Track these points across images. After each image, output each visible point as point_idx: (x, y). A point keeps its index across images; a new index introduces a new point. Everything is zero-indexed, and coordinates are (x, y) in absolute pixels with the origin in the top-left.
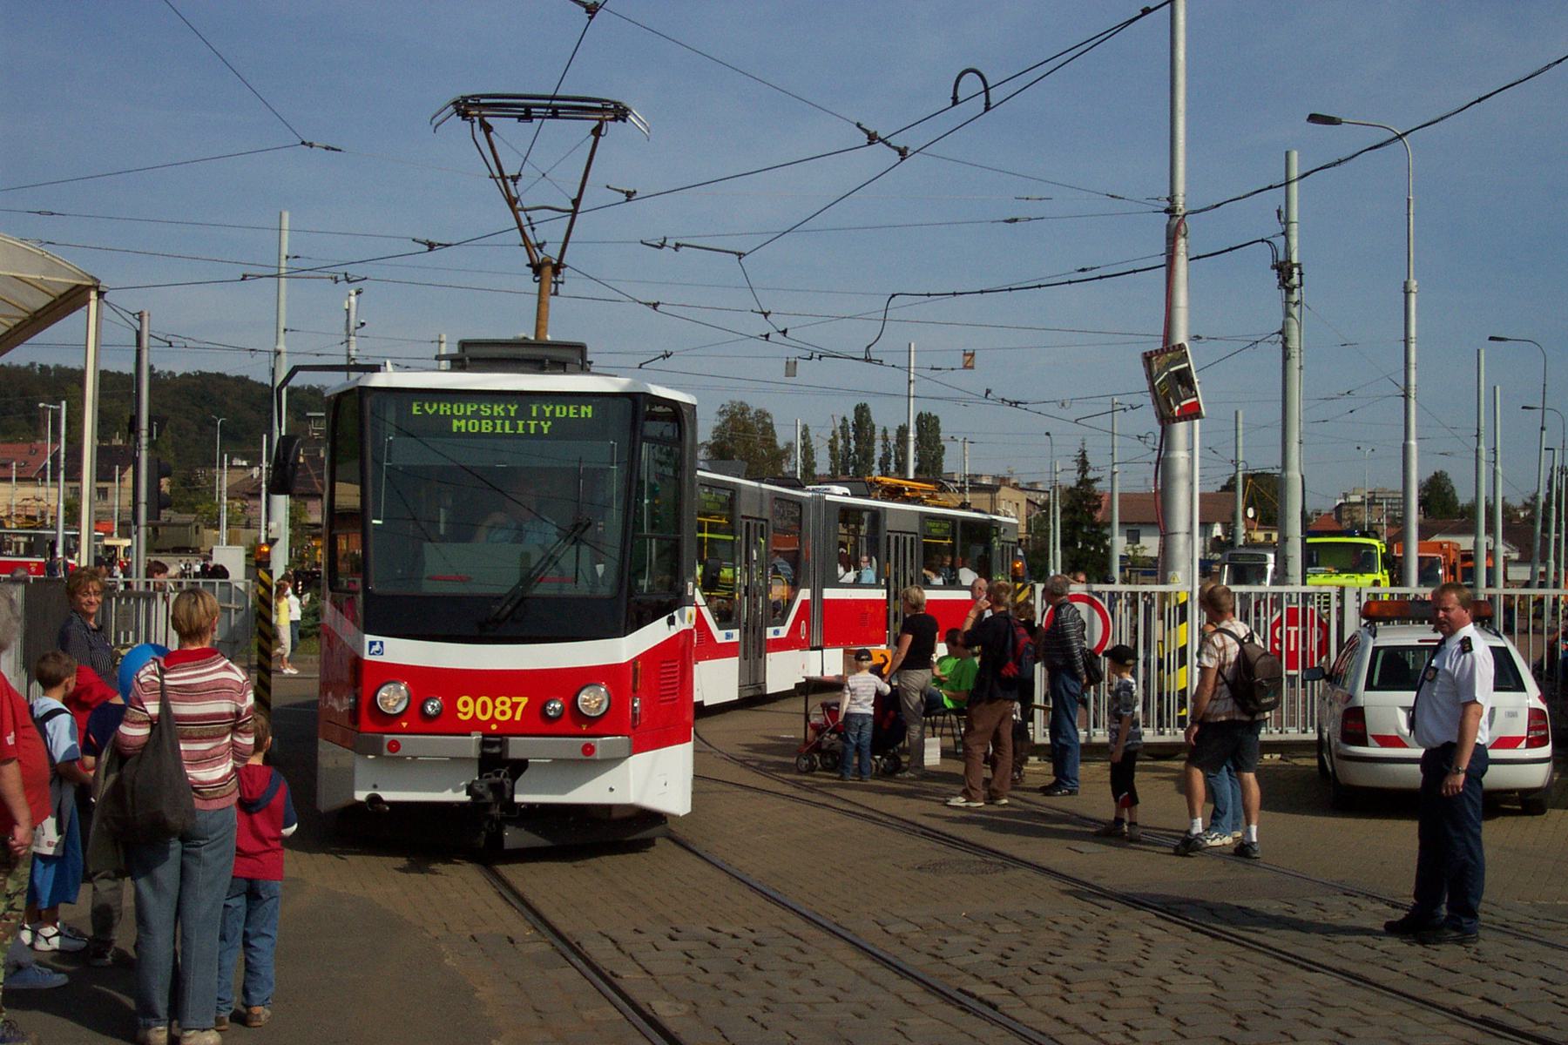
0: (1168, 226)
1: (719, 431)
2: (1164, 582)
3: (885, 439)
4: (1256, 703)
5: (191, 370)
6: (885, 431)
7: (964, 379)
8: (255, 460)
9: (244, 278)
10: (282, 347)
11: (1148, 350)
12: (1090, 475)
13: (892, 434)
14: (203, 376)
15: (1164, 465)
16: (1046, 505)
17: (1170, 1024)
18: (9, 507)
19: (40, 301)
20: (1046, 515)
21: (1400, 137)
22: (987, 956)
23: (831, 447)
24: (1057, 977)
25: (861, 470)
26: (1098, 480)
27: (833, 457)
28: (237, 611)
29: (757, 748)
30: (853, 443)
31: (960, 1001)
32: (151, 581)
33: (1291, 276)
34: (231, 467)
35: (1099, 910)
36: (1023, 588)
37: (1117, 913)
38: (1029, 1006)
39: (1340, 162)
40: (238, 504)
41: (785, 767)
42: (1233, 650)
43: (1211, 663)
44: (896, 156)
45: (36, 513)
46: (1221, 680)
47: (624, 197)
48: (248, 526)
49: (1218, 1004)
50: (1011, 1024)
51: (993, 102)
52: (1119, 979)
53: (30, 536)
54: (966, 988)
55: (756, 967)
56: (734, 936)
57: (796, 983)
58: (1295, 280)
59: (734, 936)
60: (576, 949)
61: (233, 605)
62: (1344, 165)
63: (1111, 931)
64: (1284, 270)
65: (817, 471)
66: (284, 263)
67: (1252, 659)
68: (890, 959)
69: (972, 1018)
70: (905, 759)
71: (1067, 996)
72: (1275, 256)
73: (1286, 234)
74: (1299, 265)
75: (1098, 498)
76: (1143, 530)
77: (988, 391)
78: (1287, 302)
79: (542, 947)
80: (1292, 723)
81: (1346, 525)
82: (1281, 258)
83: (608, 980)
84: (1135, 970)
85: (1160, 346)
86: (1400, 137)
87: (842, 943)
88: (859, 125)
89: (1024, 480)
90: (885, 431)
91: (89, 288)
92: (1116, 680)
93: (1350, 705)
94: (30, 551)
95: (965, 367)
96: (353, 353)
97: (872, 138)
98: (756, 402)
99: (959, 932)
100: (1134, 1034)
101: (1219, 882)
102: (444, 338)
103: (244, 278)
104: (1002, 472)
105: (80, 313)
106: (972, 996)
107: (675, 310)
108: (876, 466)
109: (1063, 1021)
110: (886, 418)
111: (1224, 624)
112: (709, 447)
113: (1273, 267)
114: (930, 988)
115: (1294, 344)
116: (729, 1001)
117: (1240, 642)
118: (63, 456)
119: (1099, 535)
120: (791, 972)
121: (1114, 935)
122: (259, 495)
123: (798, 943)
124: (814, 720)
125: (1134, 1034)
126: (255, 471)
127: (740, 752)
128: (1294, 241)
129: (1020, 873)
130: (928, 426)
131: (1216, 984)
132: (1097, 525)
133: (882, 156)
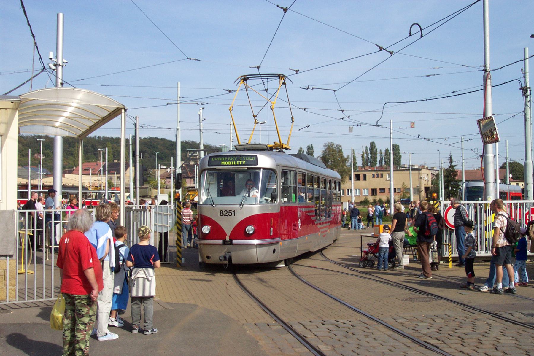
0: (484, 76)
1: (324, 152)
2: (486, 199)
3: (381, 153)
5: (146, 137)
6: (381, 151)
7: (411, 131)
8: (169, 166)
9: (168, 104)
10: (179, 127)
11: (479, 119)
12: (453, 164)
14: (150, 138)
15: (484, 157)
16: (438, 175)
18: (89, 183)
19: (105, 114)
20: (438, 179)
22: (433, 330)
24: (459, 337)
25: (373, 165)
26: (456, 165)
27: (363, 160)
28: (170, 215)
29: (345, 260)
30: (370, 155)
31: (425, 345)
32: (141, 206)
33: (527, 92)
34: (161, 168)
35: (471, 314)
36: (436, 203)
37: (477, 315)
38: (450, 347)
40: (163, 181)
41: (358, 266)
44: (389, 54)
45: (98, 185)
47: (295, 72)
48: (167, 188)
51: (424, 34)
52: (482, 338)
53: (96, 193)
55: (353, 334)
56: (344, 323)
57: (367, 339)
58: (528, 93)
59: (344, 323)
60: (291, 328)
63: (476, 321)
64: (524, 90)
65: (357, 165)
66: (179, 99)
69: (430, 351)
70: (397, 263)
71: (464, 344)
74: (529, 88)
75: (456, 172)
77: (419, 135)
78: (526, 101)
80: (481, 250)
82: (523, 86)
83: (303, 339)
84: (486, 335)
85: (482, 118)
88: (376, 45)
89: (430, 167)
90: (381, 151)
91: (122, 108)
95: (411, 127)
96: (202, 129)
97: (381, 49)
101: (513, 304)
103: (168, 104)
104: (423, 164)
105: (119, 116)
106: (430, 344)
108: (378, 163)
110: (381, 146)
112: (321, 158)
113: (520, 89)
114: (414, 341)
115: (528, 116)
116: (345, 345)
118: (107, 166)
119: (457, 185)
120: (365, 335)
121: (477, 323)
122: (170, 178)
123: (366, 326)
126: (169, 170)
127: (339, 261)
128: (528, 80)
129: (442, 301)
130: (396, 148)
131: (516, 340)
132: (456, 182)
133: (385, 54)
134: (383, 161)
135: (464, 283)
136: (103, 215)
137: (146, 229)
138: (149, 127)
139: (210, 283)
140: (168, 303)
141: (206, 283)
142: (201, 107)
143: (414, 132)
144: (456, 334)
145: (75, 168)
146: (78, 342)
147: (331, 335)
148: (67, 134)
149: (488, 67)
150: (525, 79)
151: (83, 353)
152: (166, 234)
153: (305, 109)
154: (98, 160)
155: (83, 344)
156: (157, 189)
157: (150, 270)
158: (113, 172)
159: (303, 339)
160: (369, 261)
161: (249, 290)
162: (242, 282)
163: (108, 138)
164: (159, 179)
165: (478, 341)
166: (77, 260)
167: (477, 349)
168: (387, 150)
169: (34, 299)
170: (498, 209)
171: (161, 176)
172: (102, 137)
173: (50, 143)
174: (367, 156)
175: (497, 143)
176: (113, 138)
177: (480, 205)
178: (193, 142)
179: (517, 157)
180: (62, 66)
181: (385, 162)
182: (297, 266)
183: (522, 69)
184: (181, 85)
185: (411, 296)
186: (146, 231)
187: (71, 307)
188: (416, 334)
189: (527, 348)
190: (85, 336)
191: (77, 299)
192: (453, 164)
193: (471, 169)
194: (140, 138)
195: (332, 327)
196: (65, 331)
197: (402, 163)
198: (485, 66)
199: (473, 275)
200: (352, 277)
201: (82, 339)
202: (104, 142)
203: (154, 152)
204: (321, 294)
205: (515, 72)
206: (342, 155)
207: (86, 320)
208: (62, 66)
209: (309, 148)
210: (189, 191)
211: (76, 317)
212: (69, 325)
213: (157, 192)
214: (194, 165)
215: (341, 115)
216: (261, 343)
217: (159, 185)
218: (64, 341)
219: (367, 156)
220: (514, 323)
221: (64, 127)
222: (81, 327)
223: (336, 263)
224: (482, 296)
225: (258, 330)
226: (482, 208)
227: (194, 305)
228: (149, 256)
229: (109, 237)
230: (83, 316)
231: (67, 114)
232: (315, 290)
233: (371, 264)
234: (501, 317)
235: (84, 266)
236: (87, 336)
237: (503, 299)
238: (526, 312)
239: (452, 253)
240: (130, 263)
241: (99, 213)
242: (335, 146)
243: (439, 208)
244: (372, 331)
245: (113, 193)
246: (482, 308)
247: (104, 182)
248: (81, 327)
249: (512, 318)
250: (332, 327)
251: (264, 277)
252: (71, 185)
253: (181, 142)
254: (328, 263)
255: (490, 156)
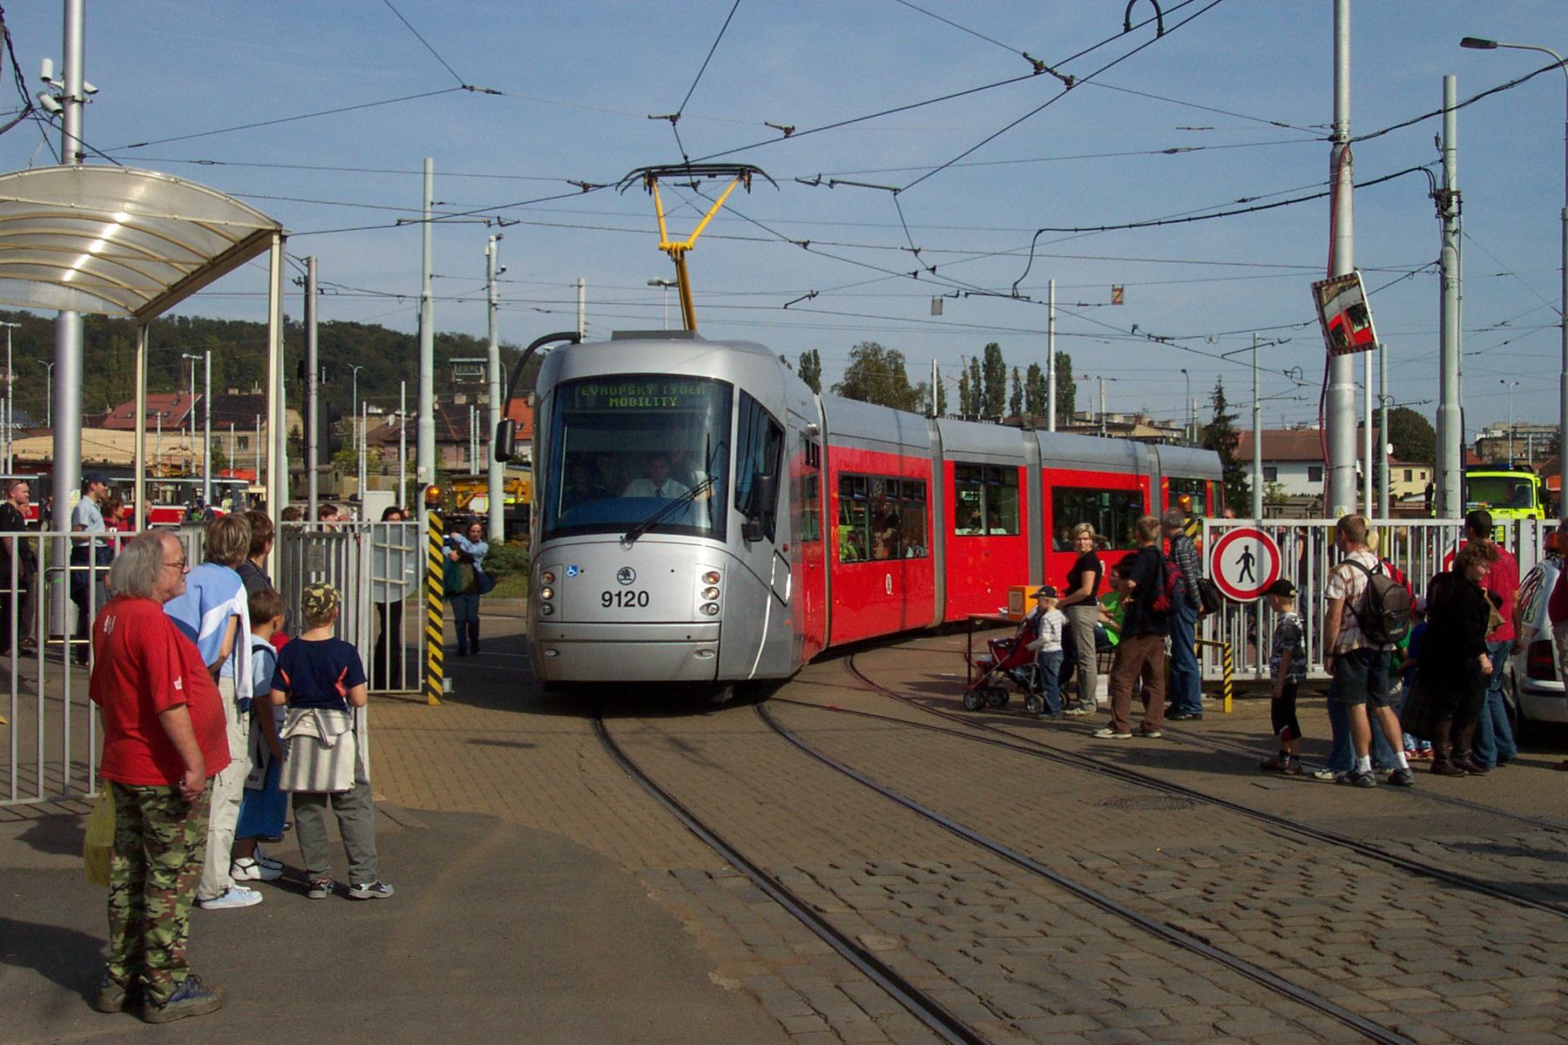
0: (1333, 154)
1: (852, 373)
3: (1016, 379)
4: (1385, 635)
6: (1016, 370)
9: (399, 223)
10: (428, 293)
12: (1228, 412)
13: (1023, 374)
15: (1329, 398)
17: (1389, 959)
18: (155, 456)
19: (220, 247)
21: (1561, 64)
23: (961, 388)
26: (1235, 417)
27: (963, 397)
28: (408, 552)
29: (921, 686)
36: (1189, 525)
37: (1313, 849)
39: (1513, 84)
40: (375, 452)
41: (962, 706)
42: (1362, 582)
43: (1338, 595)
45: (181, 462)
46: (1348, 611)
47: (782, 134)
48: (385, 473)
49: (1436, 939)
50: (1228, 959)
53: (177, 484)
54: (1174, 922)
55: (959, 902)
56: (931, 872)
57: (1000, 918)
58: (1454, 209)
59: (931, 872)
60: (776, 884)
61: (404, 547)
62: (1517, 87)
64: (1442, 198)
66: (429, 208)
67: (1381, 592)
68: (1093, 894)
69: (1183, 951)
71: (1280, 931)
72: (1433, 183)
73: (1444, 161)
74: (1457, 193)
76: (1279, 467)
77: (1135, 327)
78: (1446, 231)
79: (741, 882)
81: (1487, 460)
82: (1439, 186)
83: (813, 917)
84: (1342, 904)
85: (1324, 277)
86: (1561, 64)
87: (1041, 879)
88: (1025, 55)
90: (1016, 370)
91: (271, 232)
92: (1274, 616)
93: (1536, 639)
94: (177, 499)
95: (1114, 302)
96: (494, 299)
97: (1039, 68)
98: (888, 343)
99: (1157, 867)
100: (1354, 968)
101: (1412, 818)
102: (583, 282)
103: (399, 223)
104: (1136, 409)
105: (261, 259)
106: (1183, 930)
107: (824, 249)
108: (1007, 405)
109: (1278, 955)
110: (1016, 359)
111: (1353, 555)
115: (1453, 274)
117: (1369, 573)
122: (398, 442)
123: (996, 878)
124: (976, 658)
125: (1354, 968)
126: (391, 419)
128: (1453, 169)
130: (1063, 364)
131: (1429, 919)
132: (1234, 463)
134: (1023, 401)
135: (1269, 754)
136: (225, 547)
137: (327, 593)
138: (340, 290)
139: (533, 752)
140: (411, 811)
141: (500, 749)
142: (497, 229)
143: (1120, 318)
144: (1258, 904)
145: (109, 410)
146: (152, 924)
147: (895, 904)
148: (98, 306)
149: (1344, 128)
150: (1445, 167)
151: (169, 958)
152: (397, 607)
153: (805, 245)
154: (180, 387)
155: (169, 929)
156: (356, 474)
157: (336, 717)
158: (225, 424)
159: (813, 917)
160: (992, 691)
161: (646, 773)
162: (629, 751)
163: (211, 322)
164: (364, 446)
165: (1320, 922)
166: (134, 675)
167: (1317, 946)
168: (1034, 370)
169: (10, 797)
170: (1349, 545)
171: (369, 437)
172: (190, 318)
173: (39, 338)
174: (977, 386)
175: (1369, 352)
176: (223, 323)
177: (1316, 530)
178: (463, 337)
179: (1419, 398)
180: (82, 103)
181: (1028, 403)
182: (783, 705)
183: (1437, 139)
184: (435, 167)
185: (1122, 793)
186: (328, 600)
187: (132, 822)
188: (1143, 903)
189: (1461, 942)
190: (173, 908)
191: (145, 800)
192: (1228, 412)
193: (1279, 427)
194: (320, 325)
195: (898, 883)
196: (116, 890)
197: (1077, 409)
198: (1336, 126)
199: (1294, 732)
200: (944, 736)
201: (165, 916)
202: (201, 333)
203: (357, 365)
204: (859, 785)
205: (1417, 145)
206: (904, 380)
207: (176, 859)
208: (82, 103)
209: (806, 359)
210: (455, 482)
211: (147, 854)
212: (127, 875)
213: (357, 484)
214: (468, 404)
215: (912, 263)
216: (692, 927)
217: (363, 464)
218: (111, 923)
219: (977, 386)
220: (1419, 871)
221: (89, 283)
222: (162, 880)
223: (894, 696)
224: (1316, 797)
225: (681, 888)
226: (1322, 538)
227: (486, 816)
228: (334, 671)
229: (237, 611)
230: (165, 848)
231: (97, 247)
232: (839, 775)
233: (999, 700)
234: (1378, 854)
235: (160, 699)
236: (179, 906)
237: (1374, 803)
238: (1452, 839)
239: (1233, 671)
240: (279, 696)
241: (216, 542)
242: (885, 354)
243: (1199, 537)
244: (1012, 895)
245: (227, 486)
246: (1325, 829)
247: (199, 451)
248: (162, 880)
249: (1414, 857)
250: (898, 883)
251: (687, 736)
252: (100, 460)
253: (435, 337)
254: (873, 697)
255: (1346, 388)
